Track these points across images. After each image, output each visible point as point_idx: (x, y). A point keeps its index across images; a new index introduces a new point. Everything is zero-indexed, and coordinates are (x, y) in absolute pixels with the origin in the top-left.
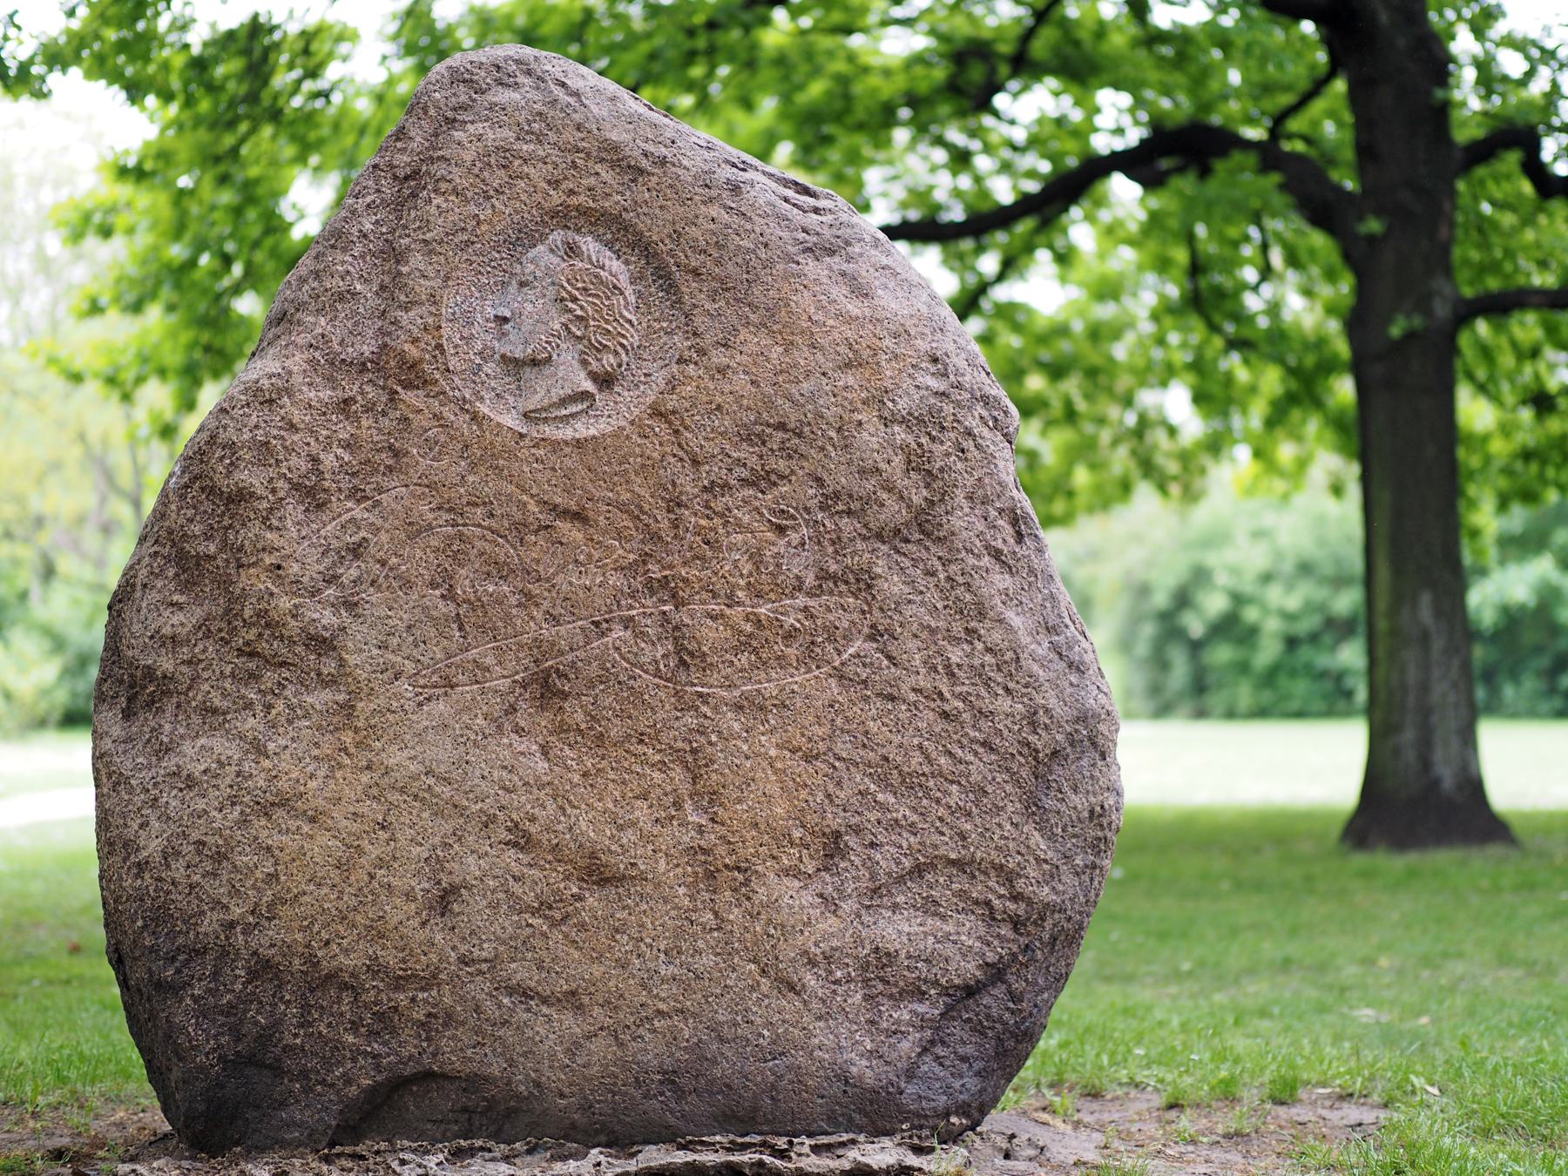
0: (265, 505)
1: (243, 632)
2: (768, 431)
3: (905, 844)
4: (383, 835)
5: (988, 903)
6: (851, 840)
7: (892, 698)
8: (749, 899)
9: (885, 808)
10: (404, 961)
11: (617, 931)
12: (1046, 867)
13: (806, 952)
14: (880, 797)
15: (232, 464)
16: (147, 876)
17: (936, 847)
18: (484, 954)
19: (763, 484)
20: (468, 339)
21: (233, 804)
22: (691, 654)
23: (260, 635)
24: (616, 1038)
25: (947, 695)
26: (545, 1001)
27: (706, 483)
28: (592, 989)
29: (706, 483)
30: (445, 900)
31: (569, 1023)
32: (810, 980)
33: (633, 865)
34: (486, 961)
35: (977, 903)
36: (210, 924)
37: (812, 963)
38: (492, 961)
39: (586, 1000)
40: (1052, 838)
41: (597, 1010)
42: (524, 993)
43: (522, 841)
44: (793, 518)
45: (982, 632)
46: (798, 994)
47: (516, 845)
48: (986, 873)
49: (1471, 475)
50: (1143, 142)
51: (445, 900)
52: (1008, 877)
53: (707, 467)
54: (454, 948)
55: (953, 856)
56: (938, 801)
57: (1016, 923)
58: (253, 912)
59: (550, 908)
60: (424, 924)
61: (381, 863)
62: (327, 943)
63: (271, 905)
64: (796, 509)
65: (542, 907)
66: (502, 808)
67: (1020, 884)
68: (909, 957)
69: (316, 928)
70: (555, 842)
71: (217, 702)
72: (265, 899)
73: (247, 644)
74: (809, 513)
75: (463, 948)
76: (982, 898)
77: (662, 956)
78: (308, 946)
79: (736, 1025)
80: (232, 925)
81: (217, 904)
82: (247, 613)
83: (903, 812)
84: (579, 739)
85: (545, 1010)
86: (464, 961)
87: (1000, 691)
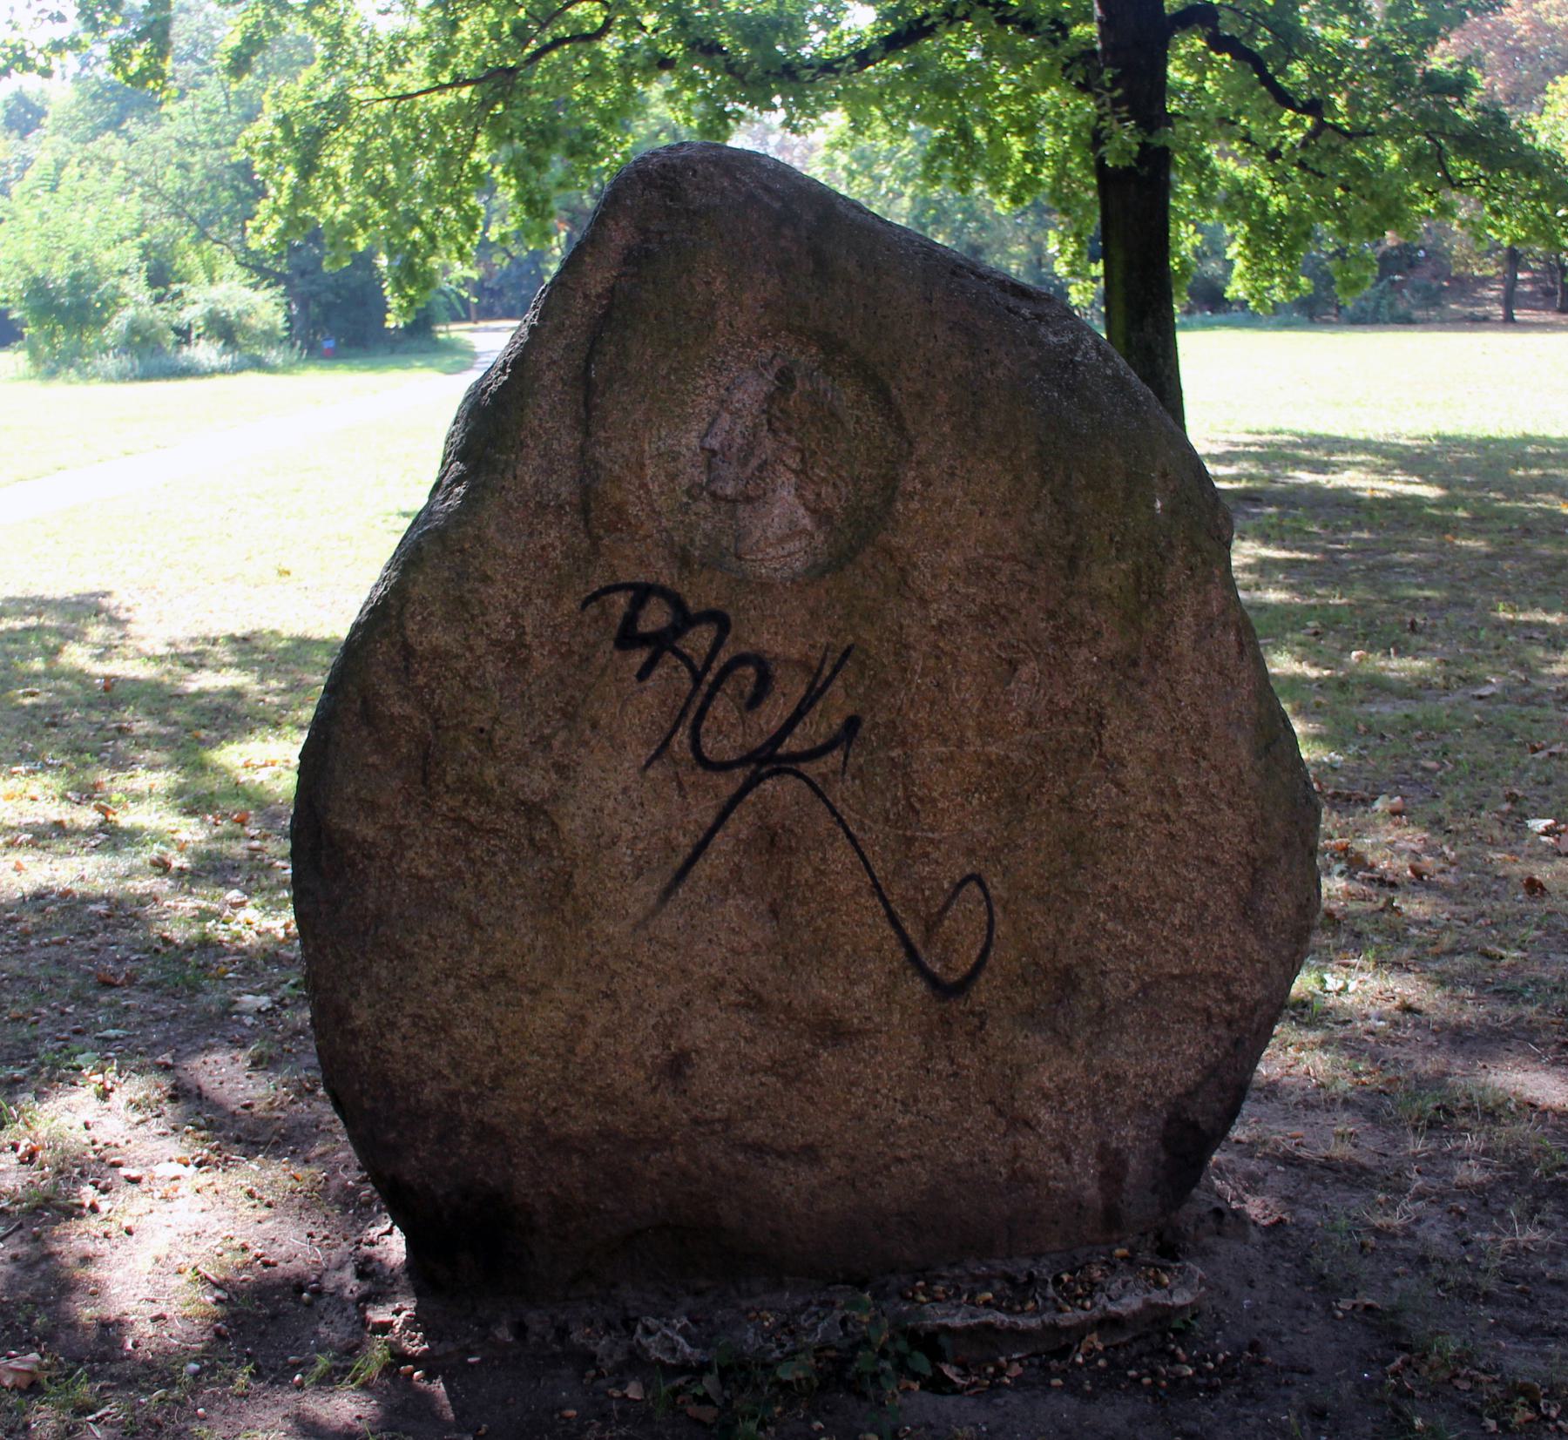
0: (462, 664)
1: (447, 798)
2: (1000, 563)
3: (1132, 967)
4: (607, 1004)
5: (1206, 1010)
6: (1082, 972)
7: (1121, 826)
8: (983, 1041)
9: (1114, 936)
10: (635, 1125)
11: (852, 1084)
12: (1259, 966)
13: (1042, 1088)
14: (1110, 926)
15: (424, 619)
16: (361, 1042)
17: (1160, 966)
18: (717, 1115)
19: (993, 619)
20: (672, 477)
21: (447, 976)
22: (921, 800)
23: (466, 801)
24: (854, 1186)
25: (1174, 817)
26: (782, 1156)
27: (934, 622)
28: (828, 1142)
29: (934, 622)
30: (677, 1067)
31: (807, 1177)
32: (1045, 1116)
33: (868, 1019)
34: (719, 1120)
35: (1196, 1011)
36: (431, 1093)
37: (1047, 1097)
38: (727, 1122)
39: (823, 1152)
40: (1264, 938)
41: (834, 1161)
42: (758, 1149)
43: (753, 1002)
44: (1021, 651)
45: (1207, 749)
46: (1032, 1128)
47: (747, 1006)
48: (1205, 982)
49: (1177, 167)
50: (1165, 76)
51: (677, 1067)
52: (1224, 981)
53: (935, 606)
54: (686, 1111)
55: (1176, 971)
56: (1163, 922)
57: (1229, 1022)
58: (474, 1083)
59: (784, 1065)
60: (654, 1089)
61: (607, 1032)
62: (555, 1110)
63: (495, 1078)
64: (1026, 642)
65: (775, 1067)
66: (731, 971)
67: (1236, 988)
68: (1136, 1075)
69: (542, 1096)
70: (786, 1001)
71: (423, 871)
72: (486, 1071)
73: (452, 810)
74: (1040, 646)
75: (696, 1111)
76: (1200, 1005)
77: (899, 1106)
78: (535, 1114)
79: (972, 1164)
80: (453, 1095)
81: (438, 1075)
82: (449, 779)
83: (1130, 938)
84: (808, 894)
85: (781, 1164)
86: (696, 1121)
87: (1223, 806)
